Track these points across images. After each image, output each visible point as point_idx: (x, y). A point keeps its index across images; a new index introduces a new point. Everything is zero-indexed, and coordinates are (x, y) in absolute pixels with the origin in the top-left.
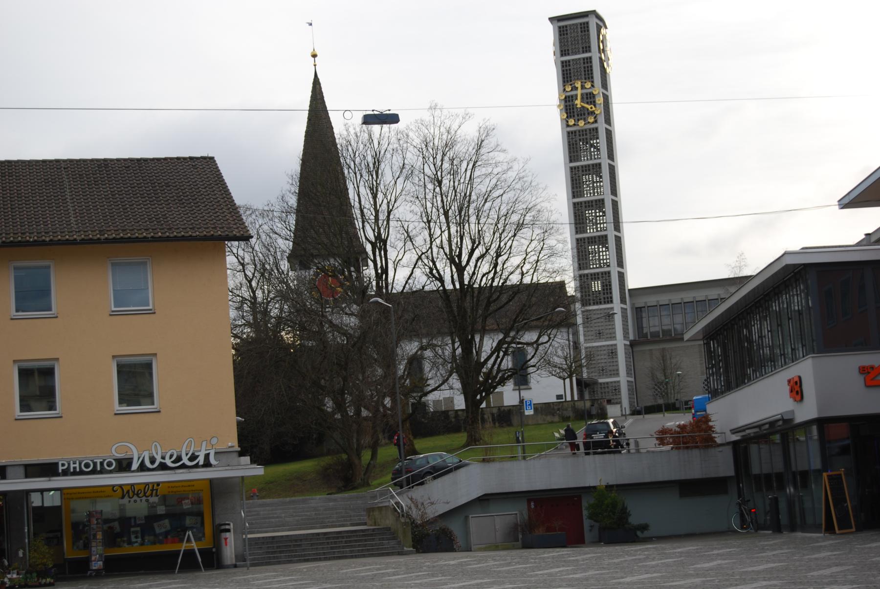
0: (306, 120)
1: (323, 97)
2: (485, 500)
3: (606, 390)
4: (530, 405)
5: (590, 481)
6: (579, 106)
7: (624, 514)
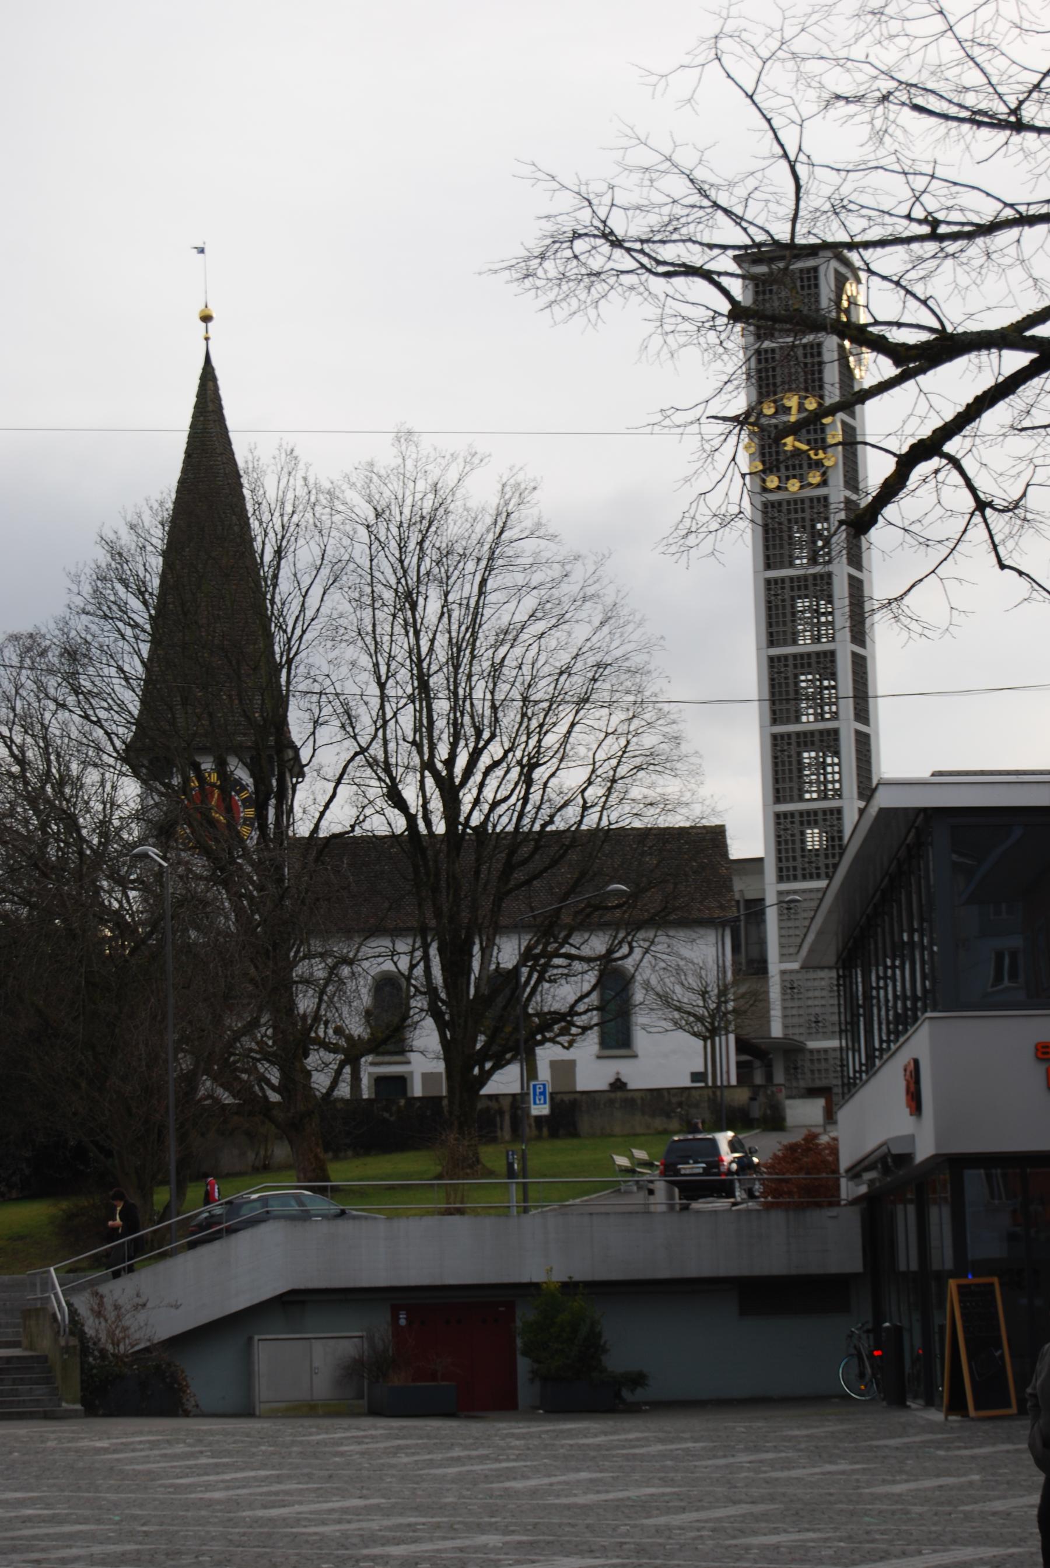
0: (182, 456)
2: (293, 1306)
3: (823, 1065)
4: (543, 1093)
5: (532, 1269)
7: (592, 1347)
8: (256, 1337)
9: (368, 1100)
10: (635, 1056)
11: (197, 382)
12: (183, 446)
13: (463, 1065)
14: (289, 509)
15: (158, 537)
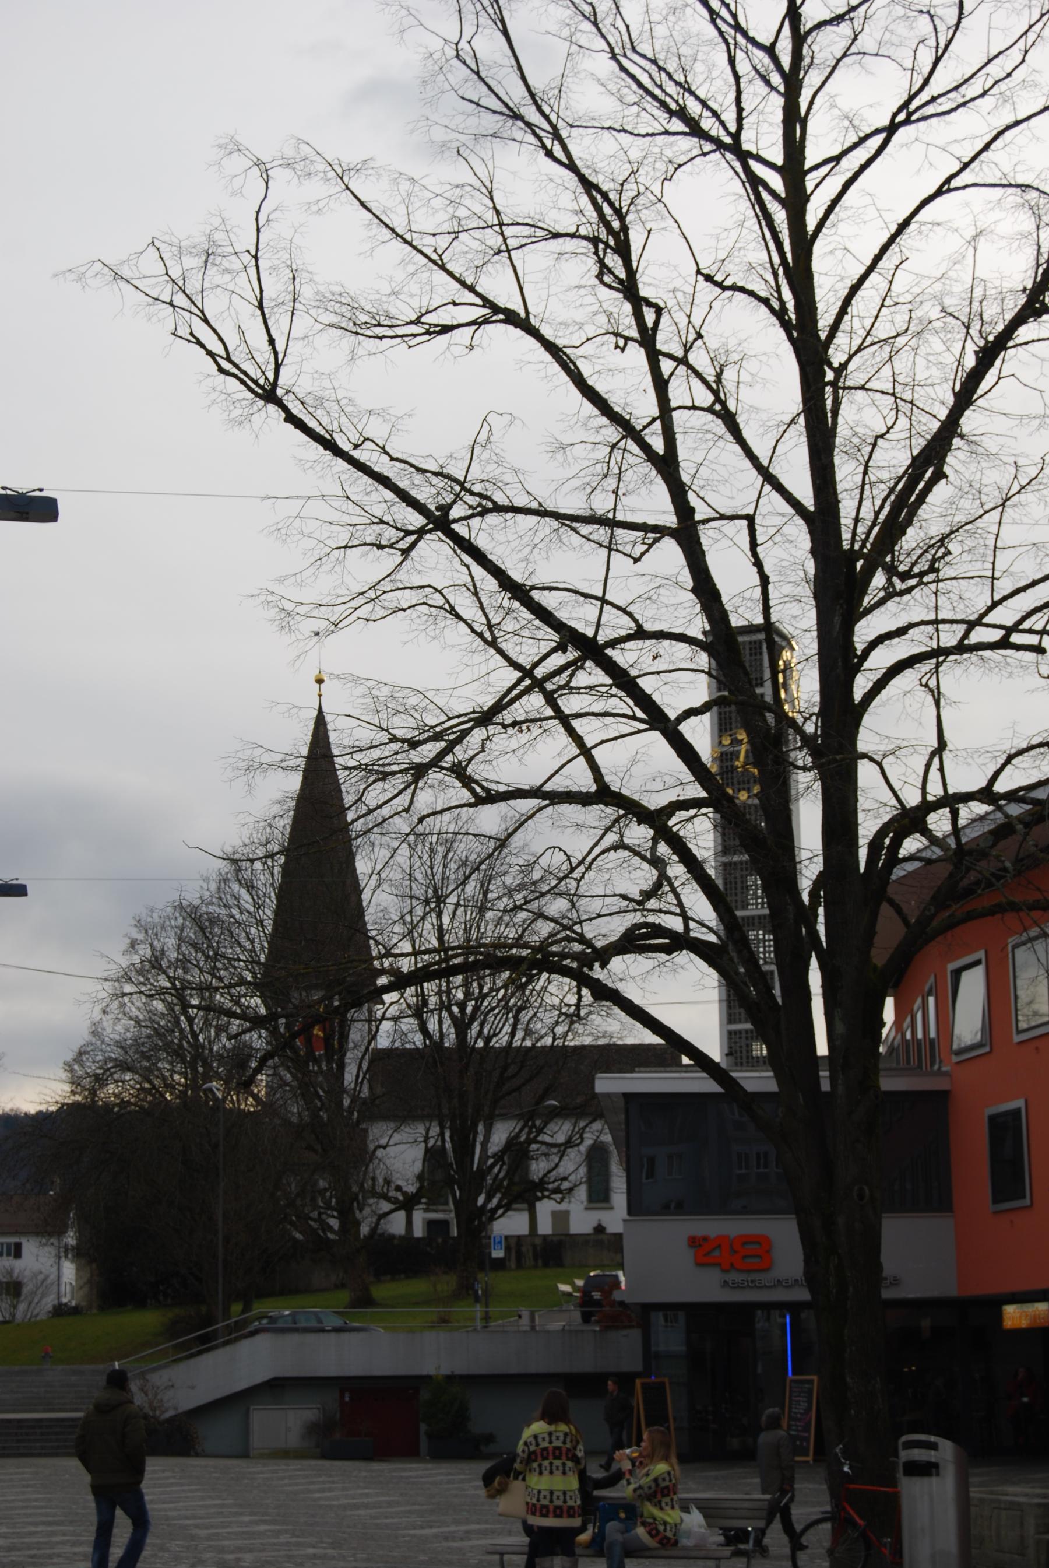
2: (276, 1388)
8: (252, 1408)
9: (418, 1239)
10: (612, 1208)
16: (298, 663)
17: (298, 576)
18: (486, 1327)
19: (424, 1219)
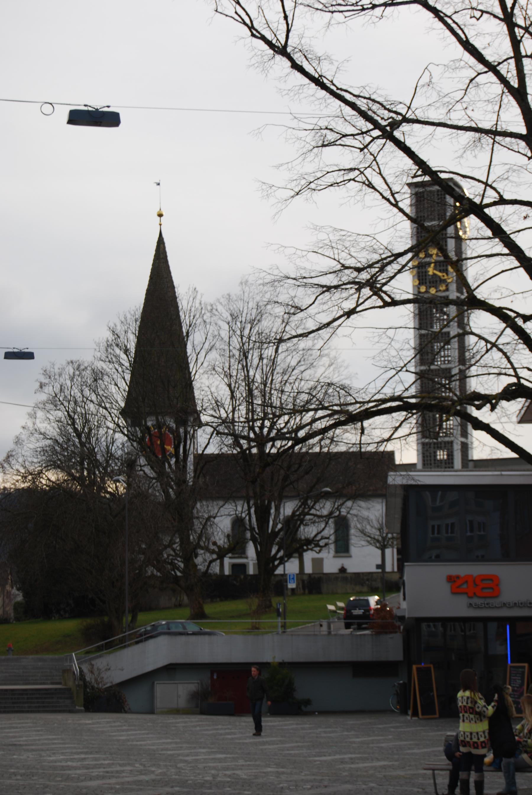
0: (148, 279)
1: (166, 256)
2: (171, 670)
5: (267, 657)
6: (431, 273)
8: (156, 682)
9: (228, 576)
10: (350, 557)
11: (156, 244)
12: (149, 274)
13: (266, 562)
14: (192, 314)
15: (134, 327)
16: (276, 217)
17: (290, 164)
18: (284, 632)
19: (229, 563)
